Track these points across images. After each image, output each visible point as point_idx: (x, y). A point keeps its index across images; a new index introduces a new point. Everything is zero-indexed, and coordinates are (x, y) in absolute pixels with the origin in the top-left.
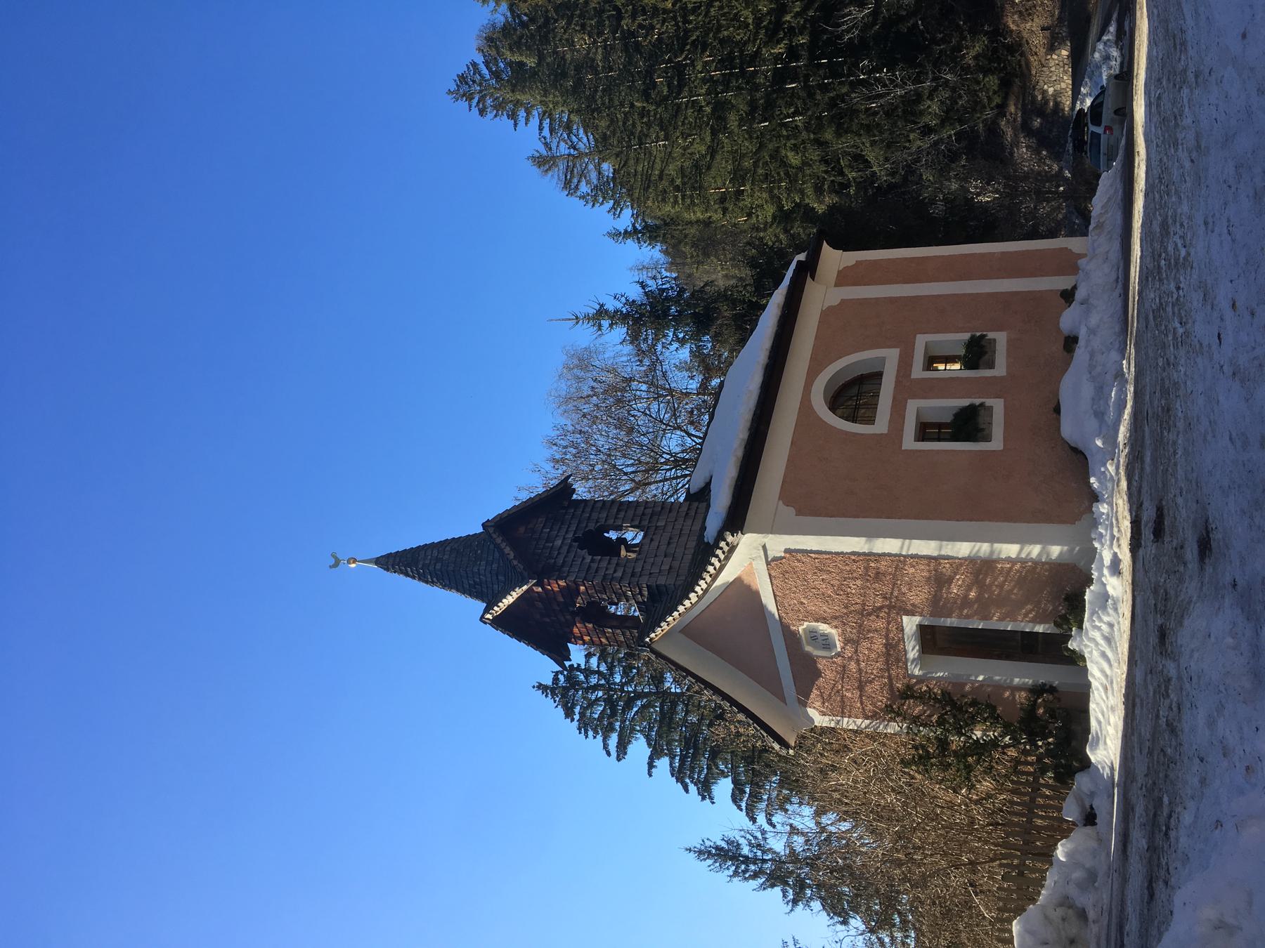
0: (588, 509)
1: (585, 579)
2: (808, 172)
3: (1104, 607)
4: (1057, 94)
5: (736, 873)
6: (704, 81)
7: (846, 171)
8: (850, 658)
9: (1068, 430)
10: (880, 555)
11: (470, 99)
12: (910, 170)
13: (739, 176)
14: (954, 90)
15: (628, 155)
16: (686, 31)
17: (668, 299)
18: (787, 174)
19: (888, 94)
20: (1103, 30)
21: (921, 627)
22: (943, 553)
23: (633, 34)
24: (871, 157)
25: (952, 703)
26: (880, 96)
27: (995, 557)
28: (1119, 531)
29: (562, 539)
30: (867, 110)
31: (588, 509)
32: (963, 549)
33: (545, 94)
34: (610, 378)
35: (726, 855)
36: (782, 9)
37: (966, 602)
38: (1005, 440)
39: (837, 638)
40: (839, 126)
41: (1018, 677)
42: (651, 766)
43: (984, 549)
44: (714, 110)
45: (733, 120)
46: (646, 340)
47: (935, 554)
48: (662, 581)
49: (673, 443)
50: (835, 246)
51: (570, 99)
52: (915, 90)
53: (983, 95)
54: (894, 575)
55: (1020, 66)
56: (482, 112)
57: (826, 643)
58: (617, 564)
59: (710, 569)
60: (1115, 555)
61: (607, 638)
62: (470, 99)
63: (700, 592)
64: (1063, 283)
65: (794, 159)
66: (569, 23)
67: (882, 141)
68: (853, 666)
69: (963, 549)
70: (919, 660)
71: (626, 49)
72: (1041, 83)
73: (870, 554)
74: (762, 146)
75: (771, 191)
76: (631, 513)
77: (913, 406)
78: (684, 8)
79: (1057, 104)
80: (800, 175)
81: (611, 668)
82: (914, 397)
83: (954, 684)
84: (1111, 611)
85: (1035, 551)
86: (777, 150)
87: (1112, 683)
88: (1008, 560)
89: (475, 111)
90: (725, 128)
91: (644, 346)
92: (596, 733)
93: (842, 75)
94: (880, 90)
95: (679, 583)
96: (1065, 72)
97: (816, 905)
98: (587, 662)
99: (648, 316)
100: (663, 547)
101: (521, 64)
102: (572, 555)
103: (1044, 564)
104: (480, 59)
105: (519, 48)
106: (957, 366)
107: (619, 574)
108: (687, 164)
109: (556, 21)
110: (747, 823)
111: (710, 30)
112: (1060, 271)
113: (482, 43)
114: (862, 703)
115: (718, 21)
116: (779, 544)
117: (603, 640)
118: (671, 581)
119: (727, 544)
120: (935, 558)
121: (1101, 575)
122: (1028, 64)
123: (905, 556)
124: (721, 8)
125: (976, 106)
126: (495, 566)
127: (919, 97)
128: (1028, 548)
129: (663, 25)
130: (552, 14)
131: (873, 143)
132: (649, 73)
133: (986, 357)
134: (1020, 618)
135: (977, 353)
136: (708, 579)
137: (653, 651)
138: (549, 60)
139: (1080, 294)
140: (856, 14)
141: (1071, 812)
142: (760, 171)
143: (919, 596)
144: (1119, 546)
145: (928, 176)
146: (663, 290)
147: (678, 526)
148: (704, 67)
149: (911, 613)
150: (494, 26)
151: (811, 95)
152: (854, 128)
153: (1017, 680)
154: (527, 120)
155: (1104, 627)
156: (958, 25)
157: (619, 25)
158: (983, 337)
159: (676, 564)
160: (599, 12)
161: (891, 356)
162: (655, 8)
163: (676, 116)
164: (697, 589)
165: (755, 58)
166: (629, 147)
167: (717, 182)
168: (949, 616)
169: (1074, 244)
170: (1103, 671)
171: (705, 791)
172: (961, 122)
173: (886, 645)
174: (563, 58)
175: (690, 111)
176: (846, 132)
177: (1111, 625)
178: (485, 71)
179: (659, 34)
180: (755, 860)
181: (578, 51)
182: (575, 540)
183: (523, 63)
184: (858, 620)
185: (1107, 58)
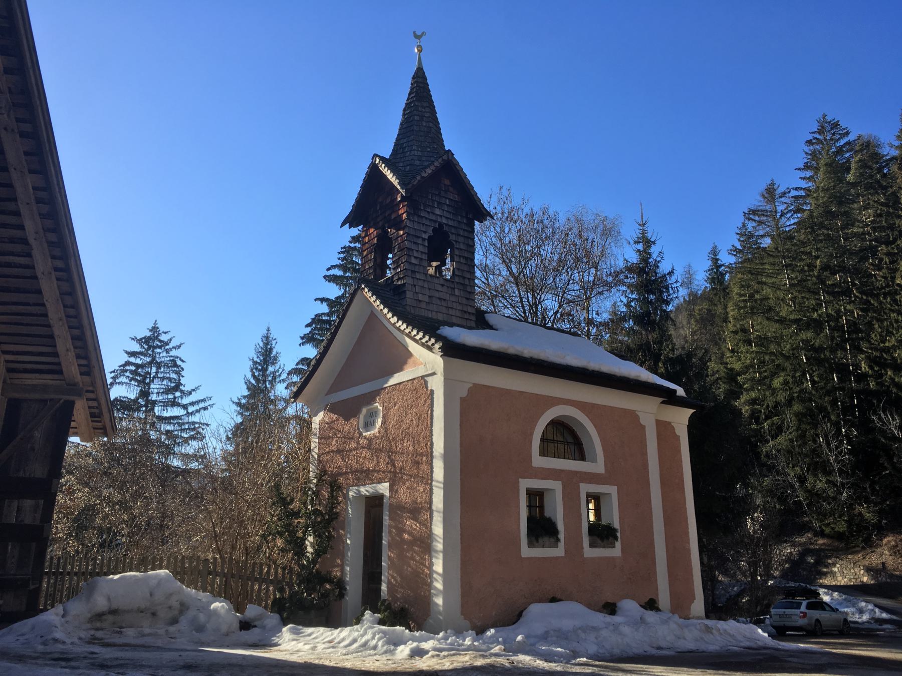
0: (466, 234)
1: (408, 234)
2: (767, 393)
3: (388, 642)
4: (833, 574)
5: (255, 363)
6: (838, 312)
7: (769, 421)
8: (358, 443)
9: (535, 609)
10: (431, 464)
11: (820, 132)
12: (771, 468)
13: (763, 341)
14: (834, 498)
15: (777, 257)
16: (878, 295)
17: (661, 292)
18: (766, 377)
19: (830, 451)
20: (883, 609)
21: (381, 497)
22: (435, 514)
23: (874, 255)
24: (780, 439)
25: (329, 522)
26: (828, 444)
27: (434, 554)
28: (445, 657)
29: (441, 214)
30: (818, 436)
31: (466, 234)
32: (438, 529)
33: (825, 190)
34: (596, 252)
35: (267, 355)
36: (898, 368)
37: (401, 531)
38: (530, 559)
39: (372, 432)
40: (804, 415)
41: (351, 571)
42: (322, 300)
43: (439, 546)
44: (815, 320)
45: (808, 335)
46: (627, 277)
47: (434, 508)
48: (409, 294)
49: (550, 303)
50: (691, 419)
51: (821, 210)
52: (834, 470)
53: (831, 519)
54: (417, 476)
55: (854, 547)
56: (809, 142)
57: (369, 425)
58: (421, 259)
59: (415, 332)
60: (427, 652)
61: (367, 255)
62: (820, 132)
63: (398, 325)
64: (664, 599)
65: (777, 382)
66: (882, 204)
67: (793, 447)
68: (353, 445)
69: (438, 529)
70: (359, 495)
71: (862, 250)
72: (841, 562)
73: (432, 457)
74: (787, 358)
75: (752, 366)
76: (465, 268)
77: (556, 486)
78: (896, 293)
79: (825, 574)
80: (765, 387)
83: (344, 522)
84: (385, 648)
85: (439, 585)
86: (784, 370)
87: (333, 647)
88: (431, 564)
89: (810, 137)
90: (800, 330)
91: (622, 276)
92: (343, 259)
93: (844, 416)
94: (833, 445)
95: (408, 308)
96: (850, 580)
97: (239, 420)
99: (648, 280)
100: (437, 295)
101: (848, 170)
102: (428, 223)
103: (430, 591)
104: (852, 137)
105: (861, 167)
106: (592, 518)
107: (413, 261)
108: (771, 302)
109: (884, 194)
110: (288, 368)
111: (879, 314)
112: (674, 595)
113: (865, 139)
114: (329, 452)
115: (886, 319)
116: (437, 384)
117: (366, 252)
118: (409, 302)
119: (433, 344)
120: (430, 508)
121: (414, 639)
122: (857, 552)
123: (431, 484)
124: (897, 321)
125: (823, 515)
126: (418, 163)
127: (828, 472)
128: (439, 578)
129: (883, 277)
130: (890, 191)
131: (791, 441)
132: (843, 269)
133: (599, 542)
134: (391, 572)
135: (602, 533)
136: (407, 331)
137: (355, 291)
138: (852, 191)
139: (650, 616)
140: (894, 424)
141: (252, 611)
142: (767, 358)
143: (404, 494)
144: (433, 656)
145: (767, 481)
146: (667, 289)
148: (849, 311)
149: (391, 489)
150: (879, 146)
151: (828, 393)
152: (803, 426)
153: (348, 569)
154: (804, 178)
155: (374, 642)
156: (886, 500)
157: (881, 243)
158: (616, 538)
159: (423, 305)
160: (892, 227)
161: (598, 466)
162: (897, 270)
163: (809, 291)
164: (400, 323)
165: (857, 349)
166: (784, 257)
167: (758, 326)
168: (391, 519)
169: (698, 606)
170: (343, 640)
171: (308, 339)
172: (808, 505)
173: (368, 470)
174: (854, 202)
175: (813, 302)
176: (799, 420)
177: (375, 648)
178: (842, 142)
179: (875, 275)
180: (265, 376)
181: (860, 213)
182: (441, 225)
183: (849, 172)
184: (383, 447)
185: (861, 611)
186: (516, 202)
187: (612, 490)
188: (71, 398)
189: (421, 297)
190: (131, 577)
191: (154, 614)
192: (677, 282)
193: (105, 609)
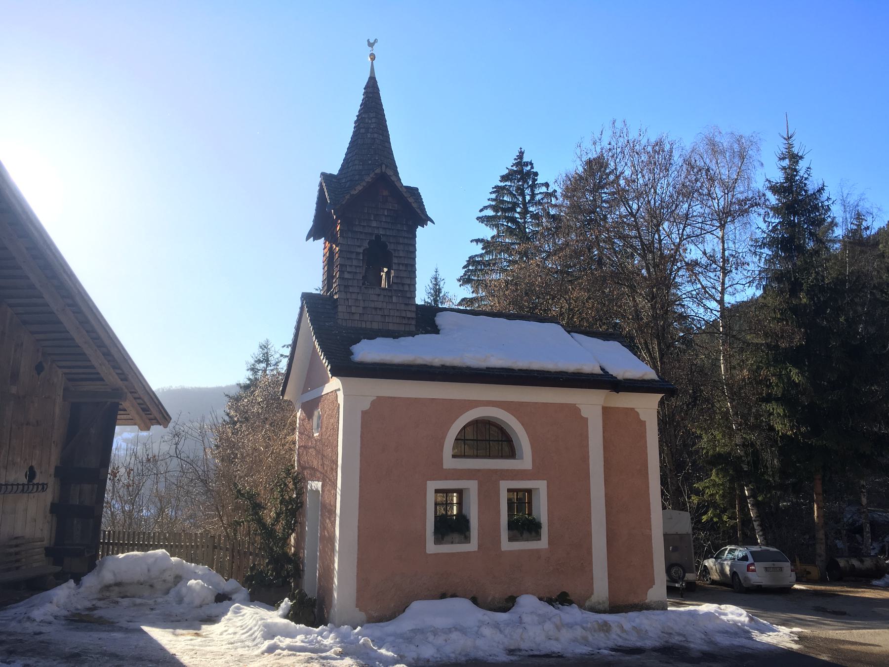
81: (539, 203)
82: (480, 486)
98: (543, 184)
147: (392, 313)
159: (357, 317)
161: (525, 461)
171: (465, 280)
182: (378, 237)
186: (633, 135)
187: (541, 486)
188: (116, 401)
189: (353, 309)
190: (133, 556)
191: (151, 586)
192: (828, 199)
193: (112, 582)
